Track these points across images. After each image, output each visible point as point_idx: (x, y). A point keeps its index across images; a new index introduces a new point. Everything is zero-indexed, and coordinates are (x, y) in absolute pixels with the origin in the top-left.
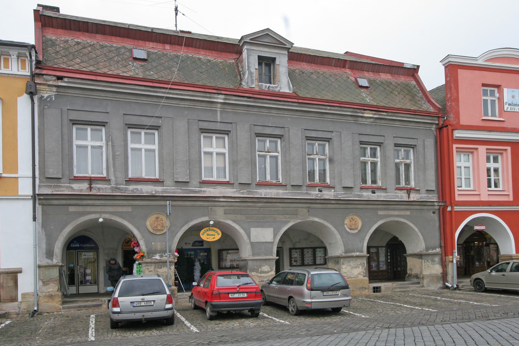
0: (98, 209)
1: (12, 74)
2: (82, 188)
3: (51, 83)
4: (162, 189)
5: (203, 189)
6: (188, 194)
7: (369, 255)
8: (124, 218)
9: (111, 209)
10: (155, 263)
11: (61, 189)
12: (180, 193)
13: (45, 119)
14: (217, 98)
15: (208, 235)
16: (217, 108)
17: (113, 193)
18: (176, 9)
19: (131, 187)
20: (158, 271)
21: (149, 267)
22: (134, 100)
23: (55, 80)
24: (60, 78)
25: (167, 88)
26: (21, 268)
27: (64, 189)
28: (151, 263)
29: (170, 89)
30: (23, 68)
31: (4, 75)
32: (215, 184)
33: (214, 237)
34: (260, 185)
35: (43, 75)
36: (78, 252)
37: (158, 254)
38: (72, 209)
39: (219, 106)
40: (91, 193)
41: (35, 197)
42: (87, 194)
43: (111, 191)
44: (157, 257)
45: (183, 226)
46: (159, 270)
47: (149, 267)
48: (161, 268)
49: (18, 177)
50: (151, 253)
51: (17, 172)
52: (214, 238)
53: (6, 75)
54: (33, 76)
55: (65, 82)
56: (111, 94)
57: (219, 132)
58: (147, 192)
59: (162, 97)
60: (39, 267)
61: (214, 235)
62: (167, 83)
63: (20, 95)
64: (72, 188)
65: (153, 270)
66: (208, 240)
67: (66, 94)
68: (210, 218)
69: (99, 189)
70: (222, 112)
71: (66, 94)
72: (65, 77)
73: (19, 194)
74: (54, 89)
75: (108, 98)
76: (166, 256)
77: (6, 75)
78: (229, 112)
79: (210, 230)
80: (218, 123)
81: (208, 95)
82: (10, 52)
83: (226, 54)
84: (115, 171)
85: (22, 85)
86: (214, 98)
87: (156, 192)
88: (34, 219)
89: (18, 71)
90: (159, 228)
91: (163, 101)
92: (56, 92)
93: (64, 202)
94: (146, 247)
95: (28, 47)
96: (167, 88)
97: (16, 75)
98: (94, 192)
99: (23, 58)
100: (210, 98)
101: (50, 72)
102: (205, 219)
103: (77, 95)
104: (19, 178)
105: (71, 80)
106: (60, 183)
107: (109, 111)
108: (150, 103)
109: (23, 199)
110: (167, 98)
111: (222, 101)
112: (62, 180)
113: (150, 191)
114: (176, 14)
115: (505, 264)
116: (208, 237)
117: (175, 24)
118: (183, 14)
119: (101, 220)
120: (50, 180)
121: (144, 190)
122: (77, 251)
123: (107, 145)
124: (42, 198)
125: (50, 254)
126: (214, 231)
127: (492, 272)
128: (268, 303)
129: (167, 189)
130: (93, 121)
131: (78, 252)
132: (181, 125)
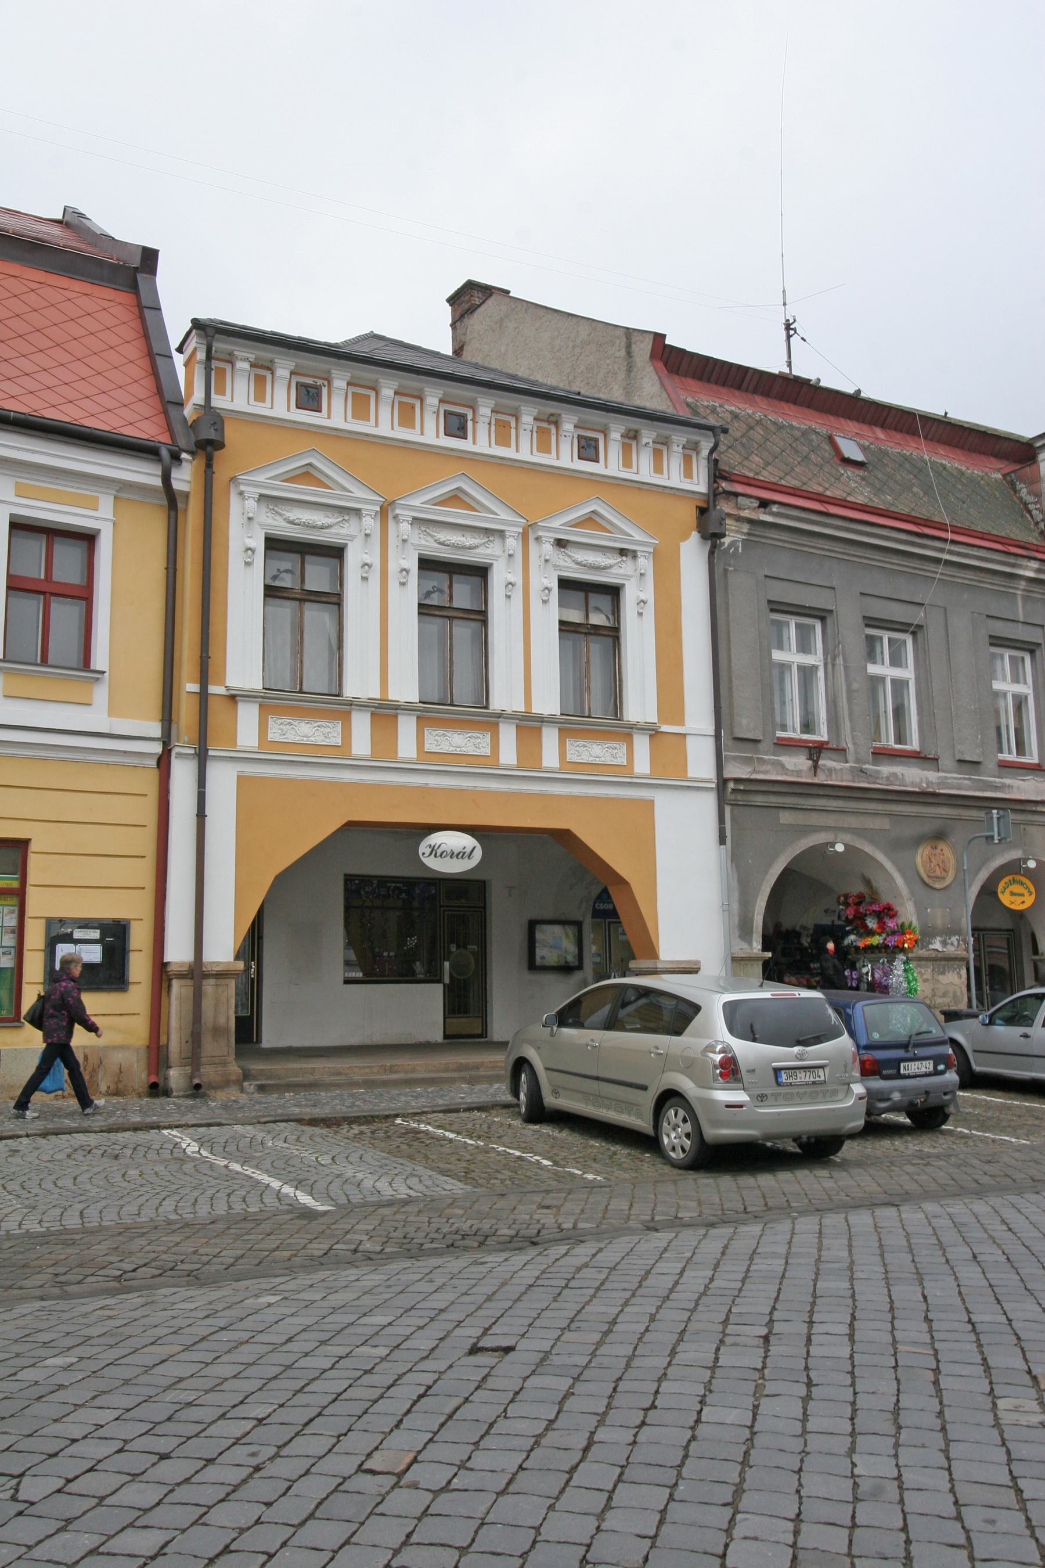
0: (831, 820)
1: (671, 488)
2: (800, 768)
3: (746, 514)
4: (939, 778)
5: (1007, 781)
6: (983, 791)
7: (769, 955)
8: (873, 842)
9: (852, 821)
10: (935, 960)
11: (765, 768)
12: (969, 789)
13: (730, 597)
14: (1026, 568)
15: (1012, 894)
16: (1017, 589)
17: (854, 781)
18: (788, 327)
19: (886, 769)
20: (939, 981)
21: (923, 971)
22: (879, 561)
23: (755, 508)
24: (764, 504)
25: (945, 540)
26: (699, 962)
27: (769, 767)
28: (927, 959)
29: (953, 542)
30: (688, 474)
31: (654, 489)
32: (1024, 771)
33: (1021, 899)
34: (881, 755)
35: (736, 495)
36: (609, 923)
37: (939, 939)
38: (786, 818)
39: (1023, 584)
40: (816, 781)
41: (722, 782)
42: (810, 781)
43: (851, 778)
44: (937, 945)
45: (979, 869)
46: (941, 978)
47: (923, 971)
48: (943, 973)
49: (685, 735)
50: (928, 934)
51: (681, 722)
52: (1023, 902)
53: (660, 490)
54: (715, 494)
55: (772, 514)
56: (841, 545)
57: (1018, 645)
58: (913, 784)
59: (937, 561)
60: (734, 959)
61: (1022, 895)
62: (942, 528)
63: (685, 537)
64: (782, 766)
65: (930, 977)
66: (1013, 907)
67: (763, 540)
68: (1024, 851)
69: (830, 770)
70: (1026, 599)
71: (763, 540)
72: (775, 502)
73: (353, 752)
74: (745, 528)
75: (833, 555)
76: (952, 944)
77: (660, 490)
78: (1038, 600)
79: (1015, 881)
80: (1020, 625)
81: (1012, 560)
82: (236, 353)
83: (983, 458)
84: (853, 729)
85: (688, 513)
86: (1020, 567)
87: (929, 783)
88: (722, 841)
89: (289, 410)
90: (938, 872)
91: (941, 569)
92: (744, 534)
93: (773, 800)
94: (919, 919)
95: (208, 329)
96: (945, 540)
97: (678, 489)
98: (821, 779)
99: (221, 365)
100: (1013, 566)
101: (749, 490)
102: (1015, 854)
103: (781, 544)
104: (688, 738)
105: (783, 510)
106: (757, 752)
107: (834, 584)
108: (905, 569)
109: (698, 789)
110: (948, 563)
111: (1031, 574)
112: (761, 746)
113: (918, 780)
114: (789, 337)
115: (1033, 999)
116: (1013, 898)
117: (786, 358)
118: (803, 339)
119: (840, 848)
120: (741, 744)
121: (908, 780)
122: (608, 920)
123: (826, 665)
124: (742, 788)
125: (745, 929)
126: (1022, 884)
127: (994, 1024)
128: (972, 1080)
129: (946, 778)
130: (810, 608)
131: (609, 923)
132: (960, 623)
